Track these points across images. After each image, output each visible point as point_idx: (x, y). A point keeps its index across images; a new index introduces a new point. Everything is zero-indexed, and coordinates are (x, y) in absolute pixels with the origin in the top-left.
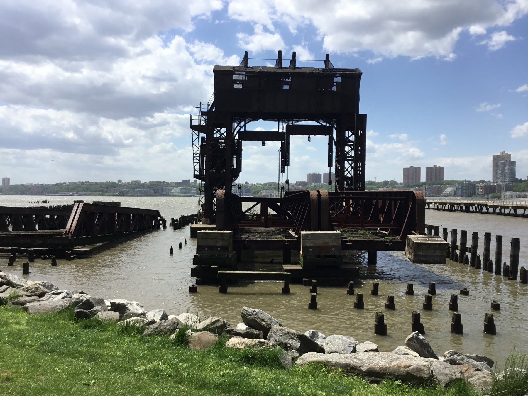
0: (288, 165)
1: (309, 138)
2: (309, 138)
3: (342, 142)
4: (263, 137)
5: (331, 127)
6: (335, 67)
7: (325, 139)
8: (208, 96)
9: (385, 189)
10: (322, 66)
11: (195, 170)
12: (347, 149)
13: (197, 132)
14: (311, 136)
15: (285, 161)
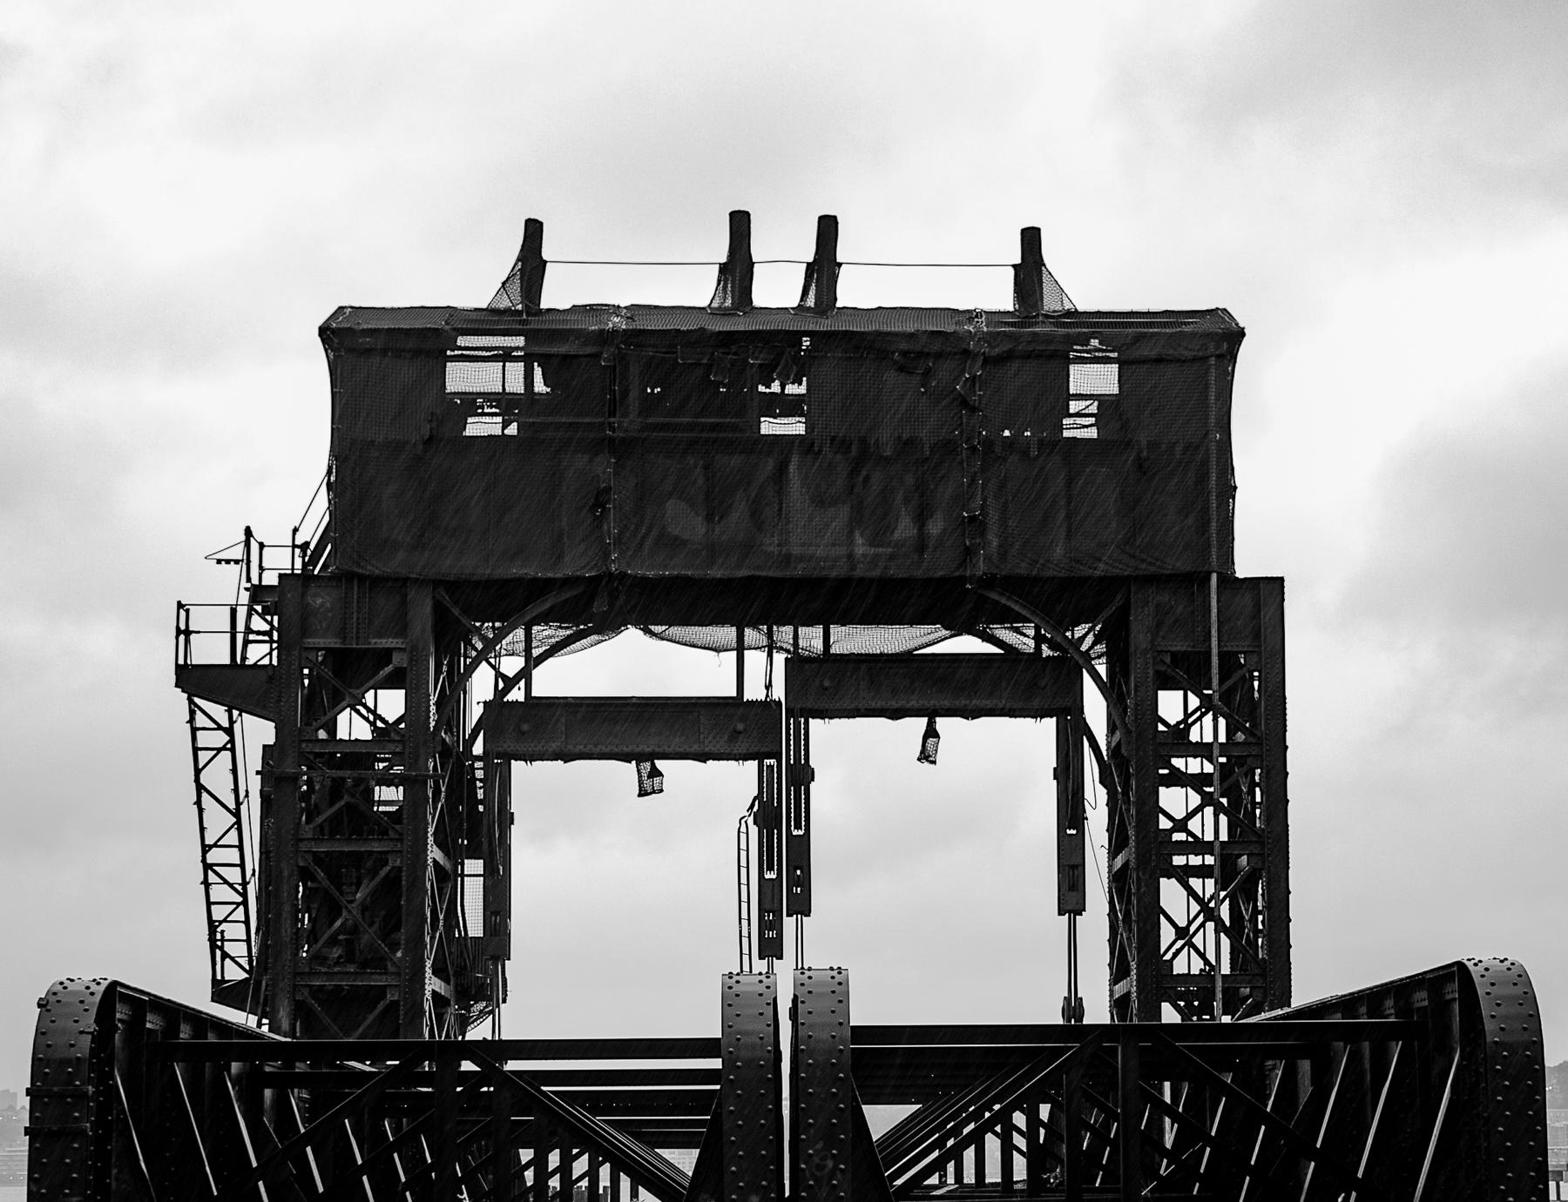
0: (802, 907)
1: (931, 733)
2: (931, 733)
3: (1140, 759)
4: (643, 732)
5: (1070, 667)
6: (1081, 308)
7: (1037, 738)
8: (289, 497)
9: (910, 328)
10: (996, 294)
11: (215, 942)
12: (1174, 800)
13: (219, 712)
14: (942, 723)
15: (783, 874)
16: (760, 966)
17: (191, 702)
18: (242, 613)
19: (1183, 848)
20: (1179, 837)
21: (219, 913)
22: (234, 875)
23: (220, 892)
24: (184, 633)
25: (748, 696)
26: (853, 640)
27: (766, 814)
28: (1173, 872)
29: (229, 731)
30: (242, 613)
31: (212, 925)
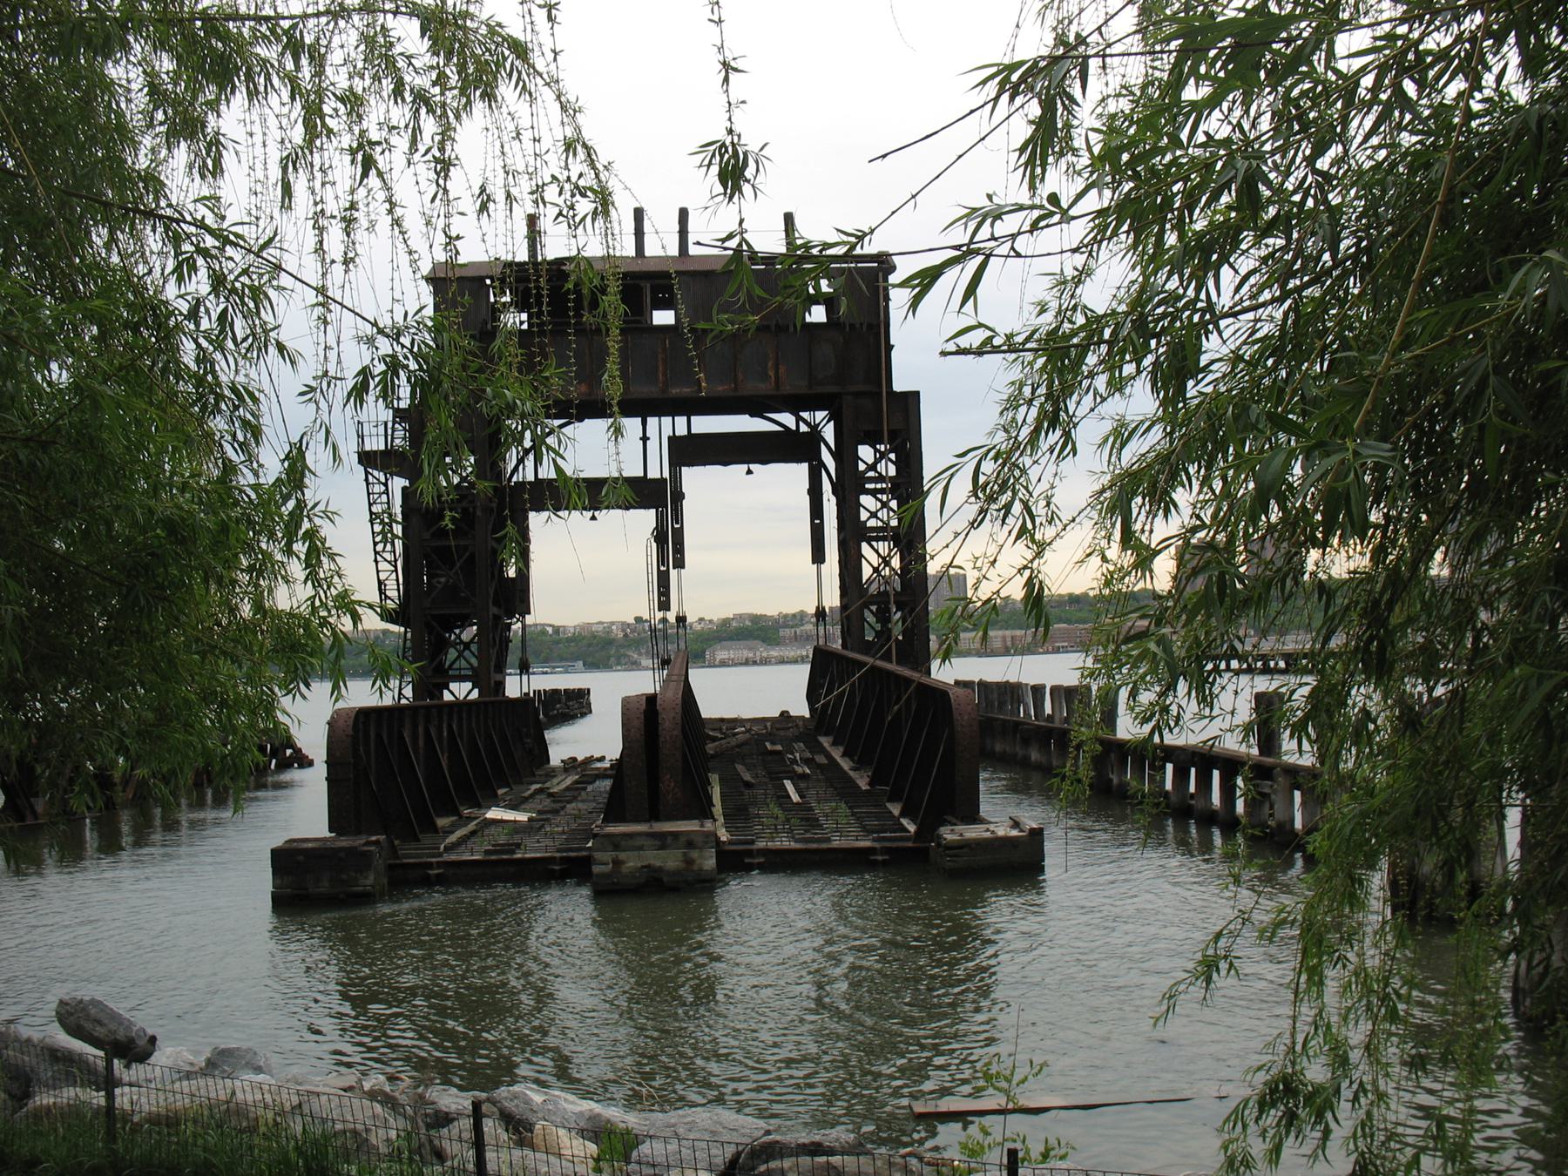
0: (680, 564)
3: (850, 486)
4: (594, 495)
16: (659, 615)
17: (367, 473)
18: (390, 425)
19: (871, 480)
20: (871, 474)
21: (383, 576)
22: (388, 556)
23: (383, 566)
24: (361, 437)
25: (650, 476)
26: (705, 424)
27: (660, 536)
28: (868, 492)
29: (386, 485)
30: (390, 425)
31: (380, 583)
